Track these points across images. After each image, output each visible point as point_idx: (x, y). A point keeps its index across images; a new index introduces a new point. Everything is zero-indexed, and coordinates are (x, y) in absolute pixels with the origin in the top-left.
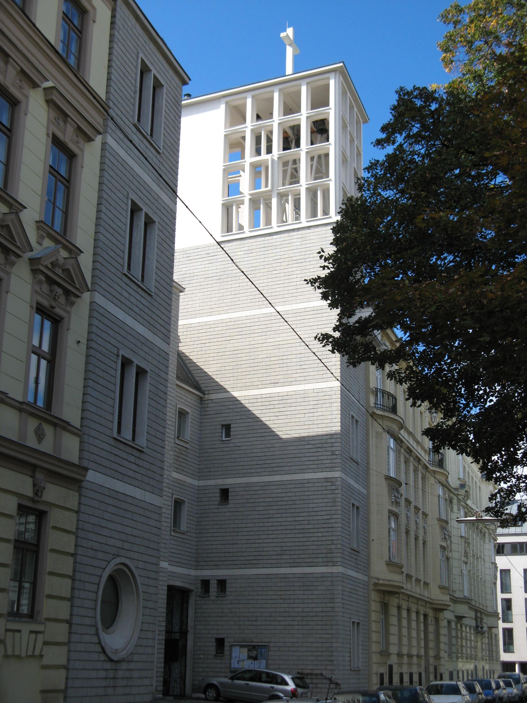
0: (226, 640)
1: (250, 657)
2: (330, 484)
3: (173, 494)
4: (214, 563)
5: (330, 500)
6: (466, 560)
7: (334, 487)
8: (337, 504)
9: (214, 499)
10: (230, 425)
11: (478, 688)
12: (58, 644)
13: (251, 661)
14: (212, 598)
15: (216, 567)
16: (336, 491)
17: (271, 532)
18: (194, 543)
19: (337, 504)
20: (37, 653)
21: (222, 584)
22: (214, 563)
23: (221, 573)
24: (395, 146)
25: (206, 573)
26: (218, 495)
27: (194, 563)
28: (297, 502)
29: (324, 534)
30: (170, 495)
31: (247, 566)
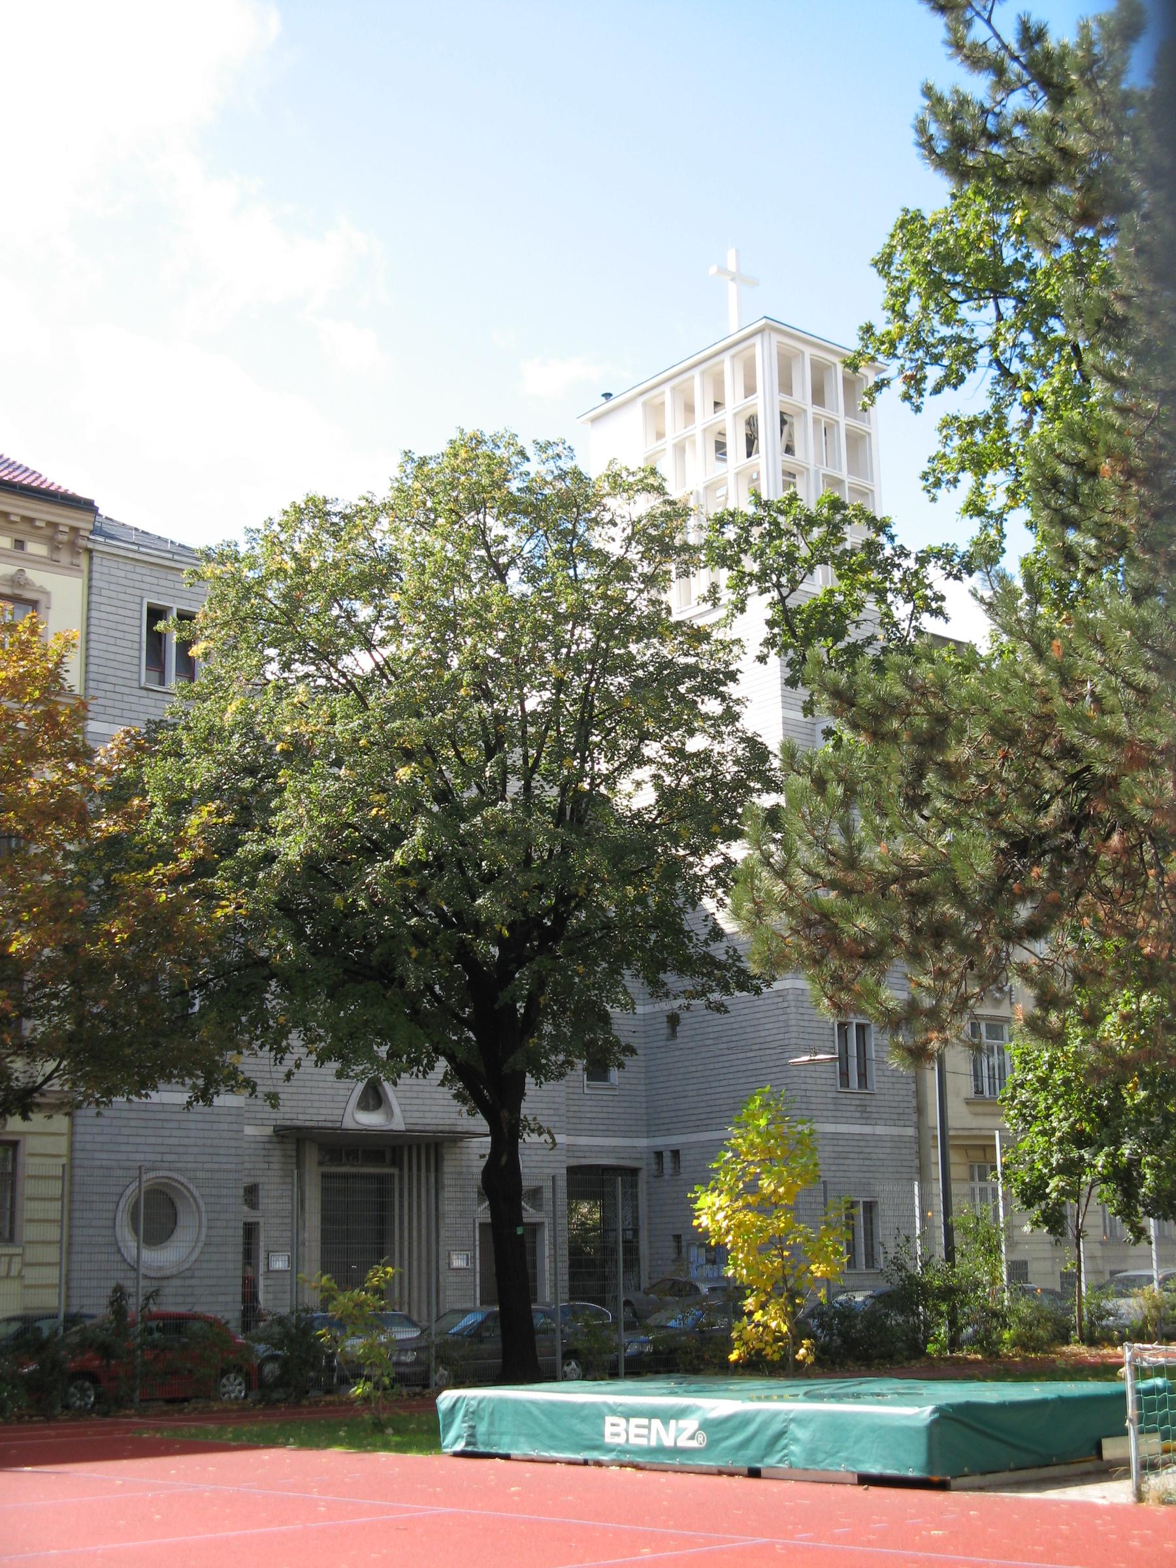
0: (683, 1238)
1: (708, 1261)
2: (780, 999)
3: (142, 598)
4: (666, 1127)
5: (781, 1024)
6: (1108, 510)
7: (785, 1004)
8: (791, 1029)
9: (662, 1032)
10: (1025, 1263)
11: (103, 976)
12: (50, 1243)
13: (709, 1266)
14: (666, 1177)
15: (669, 1132)
16: (788, 1010)
17: (722, 1077)
18: (644, 1099)
19: (791, 1029)
20: (14, 1272)
21: (676, 1154)
22: (666, 1127)
23: (674, 1140)
24: (841, 645)
25: (660, 1142)
26: (665, 1025)
27: (645, 1129)
28: (748, 1030)
29: (779, 1075)
30: (138, 600)
31: (701, 1128)
